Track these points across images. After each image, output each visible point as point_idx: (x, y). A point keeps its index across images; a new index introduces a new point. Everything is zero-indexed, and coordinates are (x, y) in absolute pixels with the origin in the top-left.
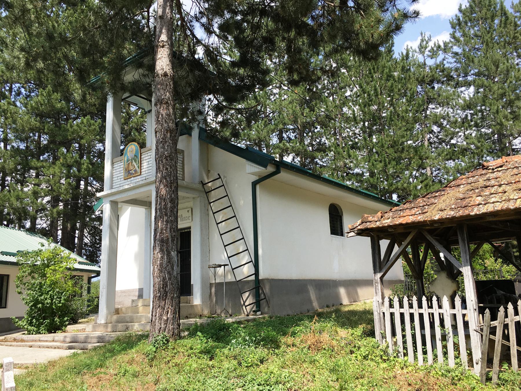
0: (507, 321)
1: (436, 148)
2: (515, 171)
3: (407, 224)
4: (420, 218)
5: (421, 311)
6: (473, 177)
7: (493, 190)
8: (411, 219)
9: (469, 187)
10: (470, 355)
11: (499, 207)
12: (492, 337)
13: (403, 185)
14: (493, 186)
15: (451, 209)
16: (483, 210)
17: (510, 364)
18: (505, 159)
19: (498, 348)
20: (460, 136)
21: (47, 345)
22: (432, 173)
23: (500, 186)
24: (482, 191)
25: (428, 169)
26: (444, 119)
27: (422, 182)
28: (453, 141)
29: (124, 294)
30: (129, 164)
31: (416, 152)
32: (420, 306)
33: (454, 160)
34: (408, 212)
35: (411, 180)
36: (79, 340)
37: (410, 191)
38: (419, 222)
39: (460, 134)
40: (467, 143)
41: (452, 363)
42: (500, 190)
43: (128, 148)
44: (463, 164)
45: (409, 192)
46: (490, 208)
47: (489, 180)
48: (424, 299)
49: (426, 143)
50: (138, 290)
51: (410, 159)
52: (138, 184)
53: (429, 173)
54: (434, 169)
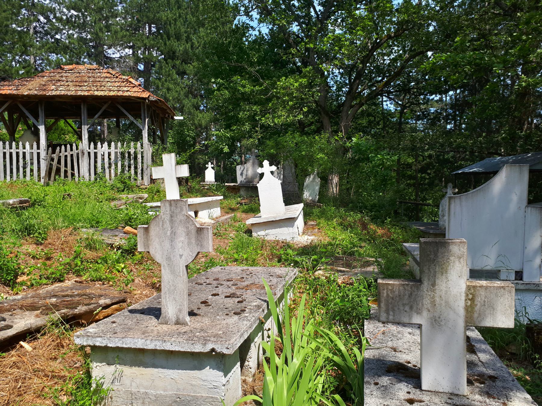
0: (61, 154)
1: (42, 38)
2: (78, 75)
3: (5, 94)
4: (15, 92)
5: (11, 151)
6: (54, 73)
7: (62, 83)
8: (8, 92)
9: (49, 79)
10: (39, 175)
11: (63, 93)
12: (51, 162)
13: (4, 67)
14: (63, 81)
15: (36, 90)
16: (54, 93)
17: (60, 176)
18: (74, 66)
19: (54, 168)
20: (64, 33)
22: (35, 61)
23: (67, 81)
24: (57, 83)
25: (32, 57)
26: (51, 13)
27: (24, 68)
28: (58, 37)
31: (20, 37)
32: (11, 148)
33: (57, 55)
34: (6, 88)
35: (14, 63)
37: (12, 74)
38: (14, 95)
39: (64, 31)
40: (69, 42)
41: (28, 178)
42: (67, 84)
44: (64, 60)
45: (10, 75)
46: (58, 93)
47: (62, 77)
48: (14, 143)
49: (32, 31)
51: (14, 43)
53: (32, 61)
54: (38, 58)
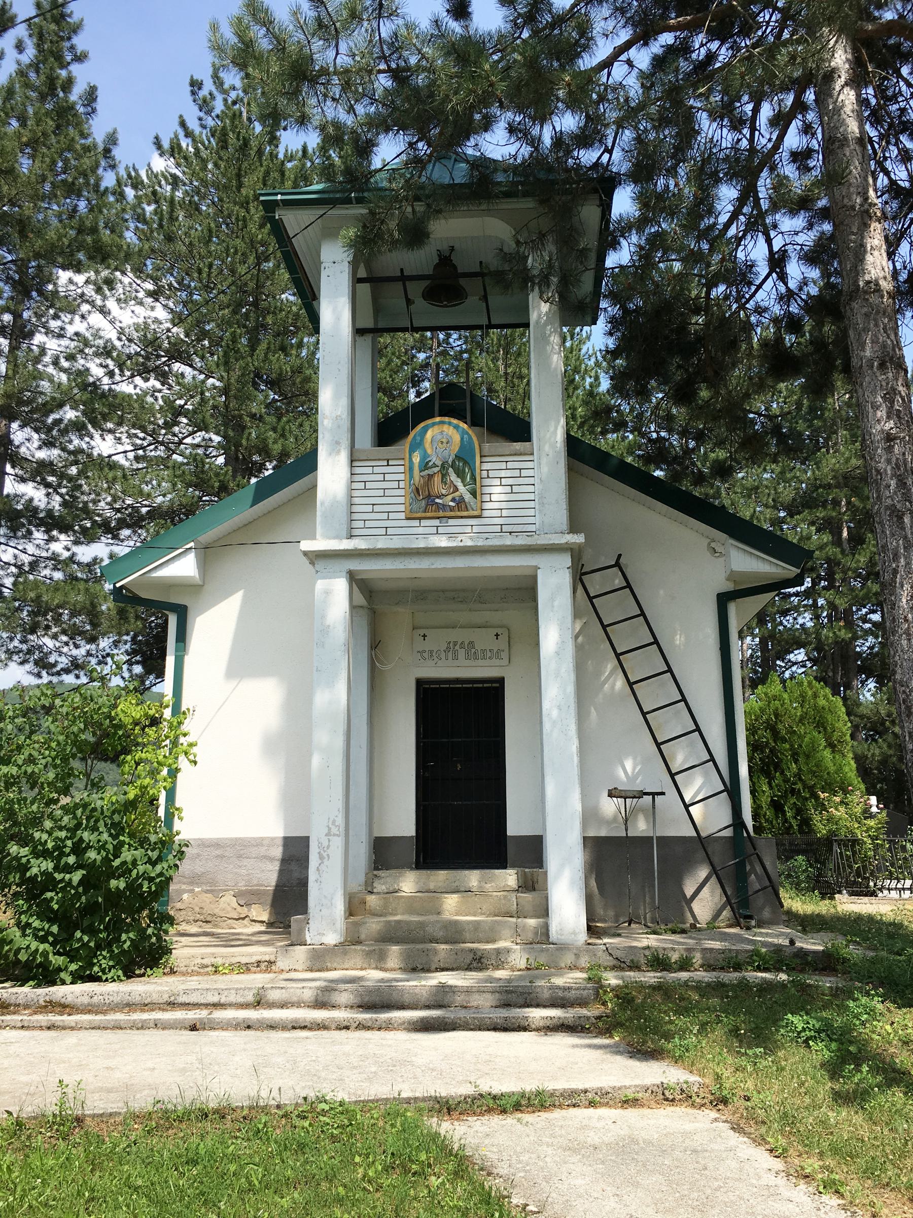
21: (296, 1021)
29: (218, 852)
30: (431, 477)
36: (407, 999)
43: (425, 430)
50: (280, 842)
52: (490, 543)
